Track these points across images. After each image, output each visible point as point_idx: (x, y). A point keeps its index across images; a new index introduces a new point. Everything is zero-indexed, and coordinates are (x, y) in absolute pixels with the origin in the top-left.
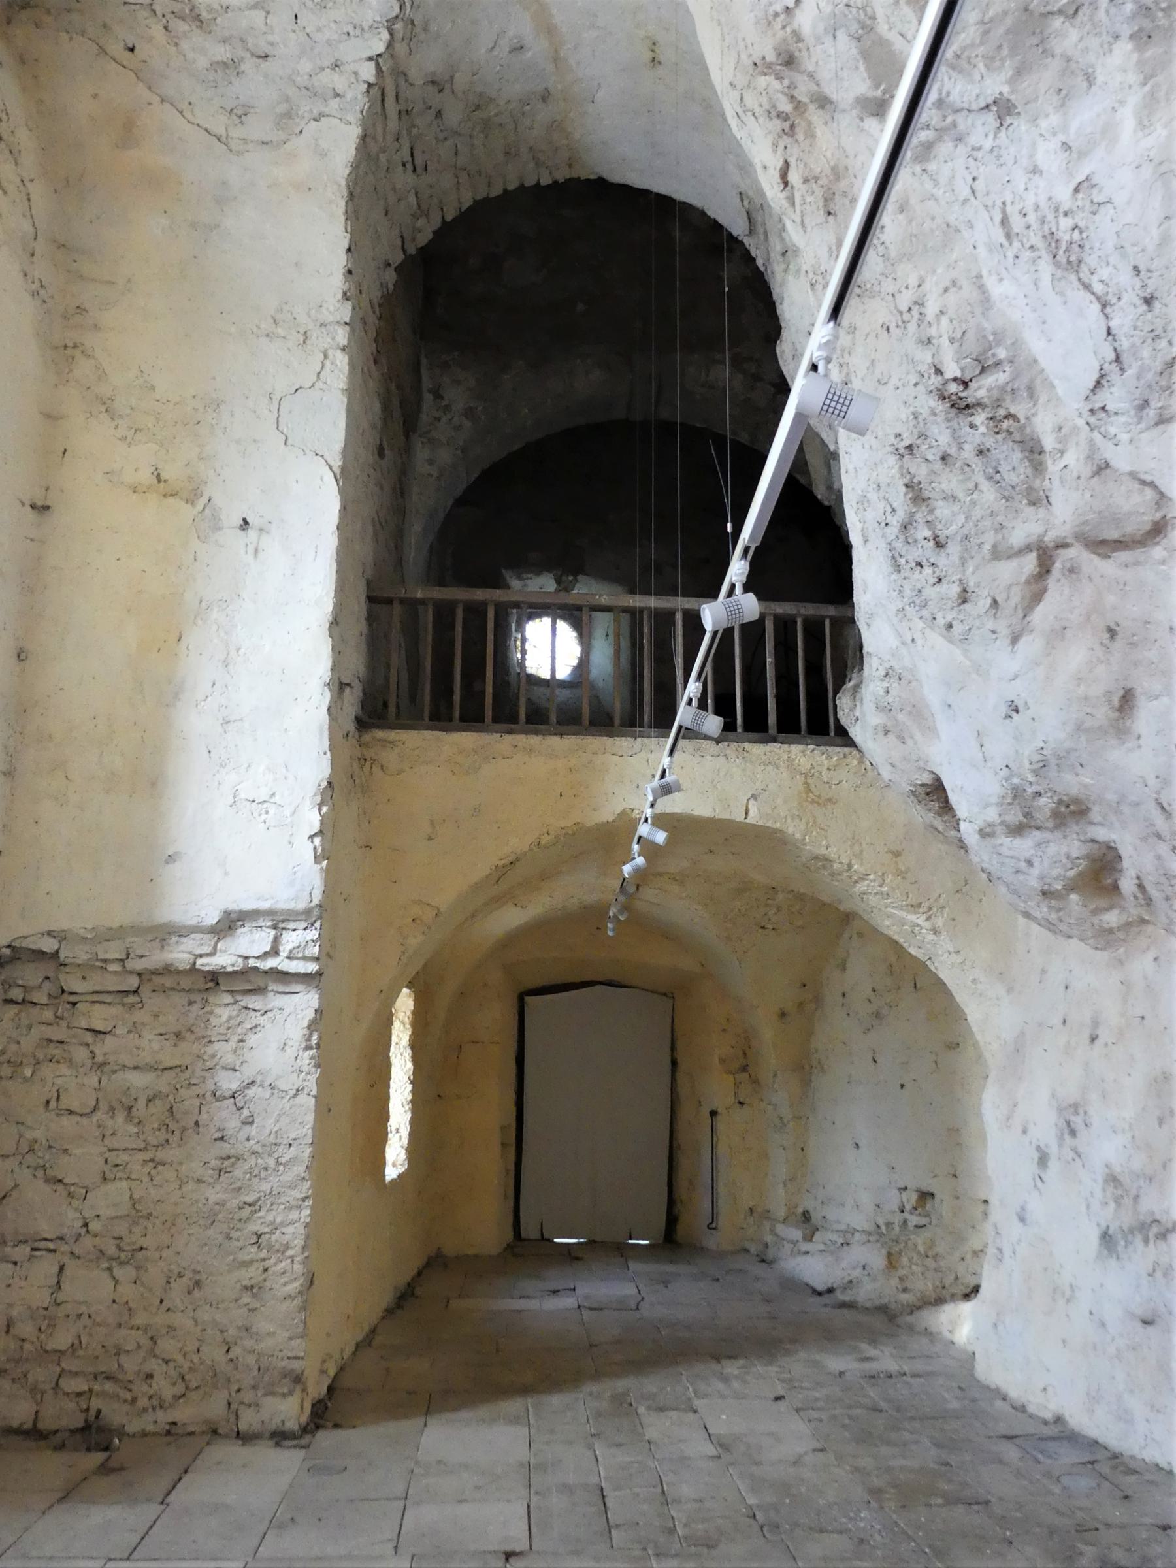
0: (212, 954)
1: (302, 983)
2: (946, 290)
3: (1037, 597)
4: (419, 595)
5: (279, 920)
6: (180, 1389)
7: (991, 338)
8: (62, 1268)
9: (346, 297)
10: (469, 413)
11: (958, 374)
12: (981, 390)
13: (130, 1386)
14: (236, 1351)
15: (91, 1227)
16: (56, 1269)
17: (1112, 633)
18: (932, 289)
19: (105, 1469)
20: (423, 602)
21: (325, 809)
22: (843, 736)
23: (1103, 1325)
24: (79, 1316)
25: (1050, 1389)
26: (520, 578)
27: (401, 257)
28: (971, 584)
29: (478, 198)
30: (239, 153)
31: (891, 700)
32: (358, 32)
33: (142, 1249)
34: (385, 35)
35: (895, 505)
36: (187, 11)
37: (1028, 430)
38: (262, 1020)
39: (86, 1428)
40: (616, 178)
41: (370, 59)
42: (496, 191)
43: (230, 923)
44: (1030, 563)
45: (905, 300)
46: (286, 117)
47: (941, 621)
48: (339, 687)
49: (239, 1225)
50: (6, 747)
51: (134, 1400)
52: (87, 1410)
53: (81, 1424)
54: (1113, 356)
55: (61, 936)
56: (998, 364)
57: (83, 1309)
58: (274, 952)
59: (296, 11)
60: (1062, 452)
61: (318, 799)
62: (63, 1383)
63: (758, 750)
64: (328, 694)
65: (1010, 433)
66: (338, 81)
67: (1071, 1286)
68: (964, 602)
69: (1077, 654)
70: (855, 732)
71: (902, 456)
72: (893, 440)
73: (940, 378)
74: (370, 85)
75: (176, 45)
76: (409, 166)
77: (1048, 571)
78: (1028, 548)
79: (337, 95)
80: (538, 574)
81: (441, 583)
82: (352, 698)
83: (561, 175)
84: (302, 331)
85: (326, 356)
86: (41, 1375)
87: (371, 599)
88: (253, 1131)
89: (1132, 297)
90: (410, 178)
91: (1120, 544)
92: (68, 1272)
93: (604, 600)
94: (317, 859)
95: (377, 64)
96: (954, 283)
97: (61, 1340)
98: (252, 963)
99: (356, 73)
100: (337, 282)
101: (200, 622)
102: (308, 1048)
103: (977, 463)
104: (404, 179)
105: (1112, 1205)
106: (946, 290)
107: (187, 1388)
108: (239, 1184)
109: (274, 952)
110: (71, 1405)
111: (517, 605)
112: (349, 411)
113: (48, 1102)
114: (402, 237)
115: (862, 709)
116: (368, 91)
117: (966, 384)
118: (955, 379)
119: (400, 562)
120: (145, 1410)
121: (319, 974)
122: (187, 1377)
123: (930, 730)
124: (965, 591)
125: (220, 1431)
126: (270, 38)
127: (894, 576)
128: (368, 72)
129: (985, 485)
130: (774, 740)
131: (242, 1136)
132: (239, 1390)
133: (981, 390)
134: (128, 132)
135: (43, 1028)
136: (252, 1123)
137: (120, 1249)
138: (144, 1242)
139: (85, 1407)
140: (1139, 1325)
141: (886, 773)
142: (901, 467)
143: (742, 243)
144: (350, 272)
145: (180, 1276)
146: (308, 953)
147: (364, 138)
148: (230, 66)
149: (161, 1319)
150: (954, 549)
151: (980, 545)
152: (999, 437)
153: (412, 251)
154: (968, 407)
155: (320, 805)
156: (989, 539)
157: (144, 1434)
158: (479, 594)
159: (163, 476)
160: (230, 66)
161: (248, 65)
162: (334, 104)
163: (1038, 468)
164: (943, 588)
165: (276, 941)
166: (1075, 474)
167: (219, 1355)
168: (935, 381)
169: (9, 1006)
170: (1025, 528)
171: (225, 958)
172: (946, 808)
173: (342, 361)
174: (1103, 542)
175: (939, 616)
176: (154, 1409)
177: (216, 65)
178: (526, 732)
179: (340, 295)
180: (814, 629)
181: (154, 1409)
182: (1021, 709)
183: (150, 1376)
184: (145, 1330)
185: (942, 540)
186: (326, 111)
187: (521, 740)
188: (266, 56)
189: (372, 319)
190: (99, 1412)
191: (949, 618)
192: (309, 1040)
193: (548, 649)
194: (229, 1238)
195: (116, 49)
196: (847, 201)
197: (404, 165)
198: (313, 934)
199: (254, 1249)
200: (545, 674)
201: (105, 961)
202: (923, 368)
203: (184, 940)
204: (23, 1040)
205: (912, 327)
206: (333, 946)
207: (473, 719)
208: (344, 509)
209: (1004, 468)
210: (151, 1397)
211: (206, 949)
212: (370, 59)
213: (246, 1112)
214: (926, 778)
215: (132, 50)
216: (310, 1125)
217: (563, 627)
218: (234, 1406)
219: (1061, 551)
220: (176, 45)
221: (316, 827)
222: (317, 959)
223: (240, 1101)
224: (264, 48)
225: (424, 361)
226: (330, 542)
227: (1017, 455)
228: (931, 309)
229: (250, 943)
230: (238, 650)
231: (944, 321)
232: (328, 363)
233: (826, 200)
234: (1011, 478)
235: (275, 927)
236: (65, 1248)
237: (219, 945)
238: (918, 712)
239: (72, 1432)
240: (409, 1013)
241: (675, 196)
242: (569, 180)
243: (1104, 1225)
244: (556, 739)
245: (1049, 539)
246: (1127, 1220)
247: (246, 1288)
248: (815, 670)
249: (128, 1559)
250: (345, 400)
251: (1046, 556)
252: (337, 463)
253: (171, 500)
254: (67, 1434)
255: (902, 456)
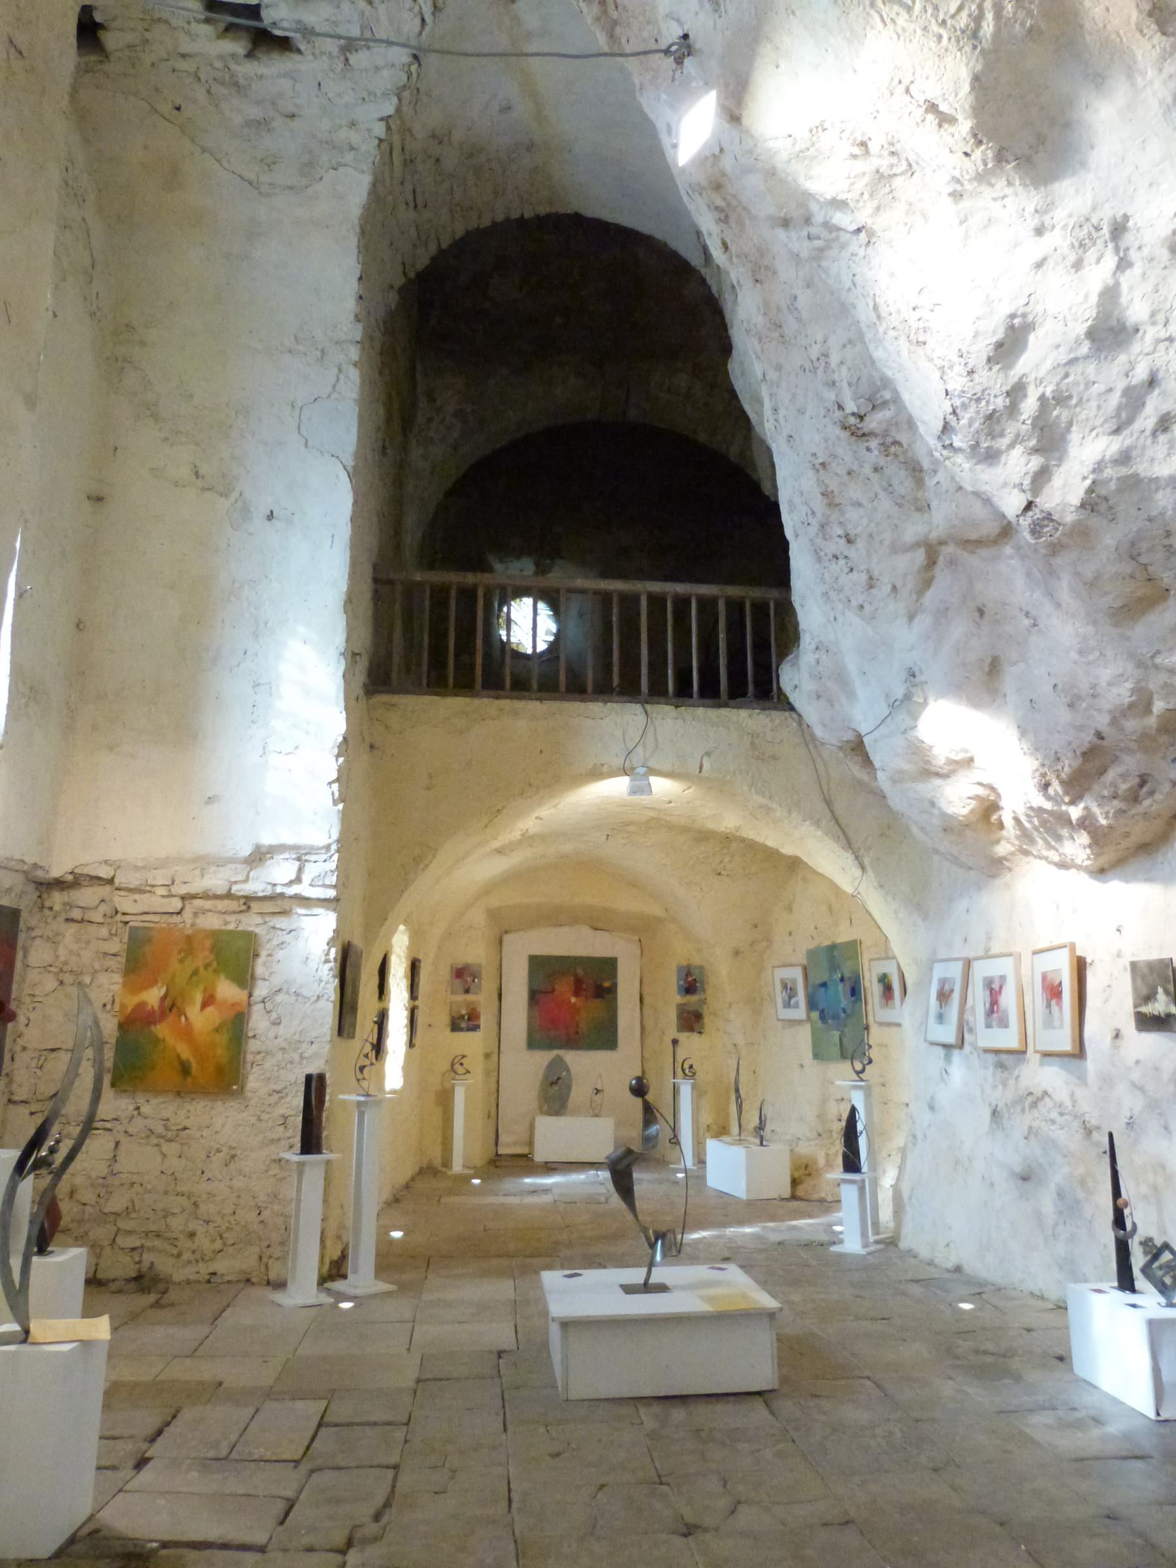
0: (246, 880)
1: (323, 907)
2: (844, 346)
3: (928, 583)
4: (418, 579)
5: (302, 855)
6: (218, 1245)
7: (879, 383)
8: (117, 1144)
9: (358, 319)
10: (459, 414)
11: (855, 410)
12: (873, 422)
13: (176, 1243)
14: (266, 1213)
15: (142, 1110)
16: (112, 1145)
17: (981, 612)
18: (834, 344)
19: (157, 1305)
20: (421, 584)
21: (341, 760)
22: (787, 706)
23: (992, 1185)
24: (132, 1184)
25: (952, 1245)
26: (501, 561)
27: (403, 280)
28: (876, 574)
29: (469, 228)
30: (268, 195)
31: (821, 669)
32: (372, 98)
33: (185, 1128)
34: (395, 100)
35: (814, 509)
36: (227, 78)
37: (910, 454)
38: (288, 938)
39: (138, 1278)
40: (590, 212)
41: (382, 119)
42: (486, 222)
43: (260, 856)
44: (920, 556)
45: (815, 351)
46: (309, 166)
47: (854, 603)
48: (352, 656)
49: (268, 1109)
50: (68, 703)
51: (179, 1255)
52: (140, 1262)
53: (134, 1274)
54: (951, 410)
55: (117, 866)
56: (885, 403)
57: (135, 1178)
58: (298, 880)
59: (319, 79)
60: (935, 472)
61: (336, 751)
62: (119, 1240)
63: (713, 714)
64: (343, 662)
65: (896, 456)
66: (355, 137)
67: (969, 1158)
68: (871, 587)
69: (958, 629)
70: (794, 698)
71: (818, 470)
72: (809, 457)
73: (841, 413)
74: (381, 140)
75: (217, 106)
76: (412, 204)
77: (934, 563)
78: (917, 544)
79: (352, 148)
80: (518, 557)
81: (431, 566)
82: (363, 664)
83: (543, 210)
84: (320, 348)
85: (340, 370)
86: (102, 1233)
87: (376, 580)
88: (281, 1030)
89: (960, 369)
90: (412, 214)
91: (979, 543)
92: (122, 1148)
93: (579, 583)
94: (335, 803)
95: (387, 123)
96: (850, 342)
97: (116, 1204)
98: (279, 890)
99: (369, 130)
100: (350, 305)
101: (233, 599)
102: (327, 961)
103: (875, 477)
104: (407, 216)
105: (1000, 1088)
106: (844, 346)
107: (224, 1244)
108: (268, 1075)
109: (298, 880)
110: (125, 1259)
111: (503, 588)
112: (361, 418)
113: (105, 1005)
114: (404, 264)
115: (795, 677)
116: (379, 146)
117: (861, 418)
118: (853, 414)
119: (398, 547)
120: (189, 1262)
121: (337, 900)
122: (225, 1235)
123: (851, 695)
124: (871, 578)
125: (254, 1280)
126: (298, 101)
127: (817, 566)
128: (380, 130)
129: (882, 495)
130: (726, 705)
131: (271, 1034)
132: (268, 1246)
133: (873, 422)
134: (173, 177)
135: (101, 943)
136: (279, 1024)
137: (166, 1128)
138: (187, 1123)
139: (137, 1259)
140: (1020, 1182)
141: (819, 732)
142: (818, 480)
143: (699, 271)
144: (361, 297)
145: (219, 1151)
146: (327, 882)
147: (374, 184)
148: (260, 125)
149: (204, 1187)
150: (861, 544)
151: (881, 542)
152: (889, 458)
153: (412, 275)
154: (864, 435)
155: (337, 756)
156: (888, 536)
157: (189, 1282)
158: (470, 578)
159: (202, 472)
160: (260, 125)
161: (278, 123)
162: (349, 157)
163: (919, 482)
164: (855, 576)
165: (300, 870)
166: (944, 489)
167: (252, 1216)
168: (838, 414)
169: (71, 924)
170: (914, 529)
171: (256, 886)
172: (867, 762)
173: (354, 375)
174: (967, 541)
175: (852, 599)
176: (197, 1261)
177: (249, 123)
178: (511, 698)
179: (352, 317)
180: (760, 609)
181: (197, 1261)
182: (917, 674)
183: (192, 1235)
184: (189, 1197)
185: (852, 537)
186: (343, 161)
187: (505, 703)
188: (293, 116)
189: (378, 334)
190: (152, 1263)
191: (860, 602)
192: (327, 954)
193: (528, 625)
194: (259, 1119)
195: (166, 109)
196: (769, 274)
197: (407, 204)
198: (332, 865)
199: (281, 1129)
200: (530, 651)
201: (153, 886)
202: (829, 405)
203: (221, 869)
204: (83, 953)
205: (820, 372)
206: (347, 877)
207: (464, 686)
208: (355, 503)
209: (895, 482)
210: (194, 1252)
211: (240, 877)
212: (382, 119)
213: (274, 1015)
214: (849, 736)
215: (178, 109)
216: (328, 1026)
217: (541, 606)
218: (265, 1260)
219: (943, 548)
220: (217, 106)
221: (335, 776)
222: (335, 887)
223: (269, 1006)
224: (292, 109)
225: (419, 367)
226: (344, 531)
227: (903, 473)
228: (834, 359)
229: (280, 872)
230: (266, 624)
231: (844, 370)
232: (342, 377)
233: (754, 271)
234: (902, 490)
235: (299, 859)
236: (118, 1127)
237: (252, 873)
238: (841, 678)
239: (128, 1281)
240: (404, 948)
241: (640, 229)
242: (548, 216)
243: (994, 1104)
244: (537, 703)
245: (934, 535)
246: (1010, 1096)
247: (274, 1161)
248: (762, 646)
249: (191, 1356)
250: (357, 409)
251: (932, 552)
252: (350, 463)
253: (208, 494)
254: (122, 1283)
255: (818, 470)
